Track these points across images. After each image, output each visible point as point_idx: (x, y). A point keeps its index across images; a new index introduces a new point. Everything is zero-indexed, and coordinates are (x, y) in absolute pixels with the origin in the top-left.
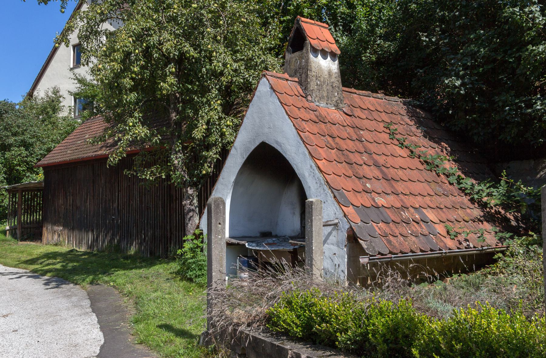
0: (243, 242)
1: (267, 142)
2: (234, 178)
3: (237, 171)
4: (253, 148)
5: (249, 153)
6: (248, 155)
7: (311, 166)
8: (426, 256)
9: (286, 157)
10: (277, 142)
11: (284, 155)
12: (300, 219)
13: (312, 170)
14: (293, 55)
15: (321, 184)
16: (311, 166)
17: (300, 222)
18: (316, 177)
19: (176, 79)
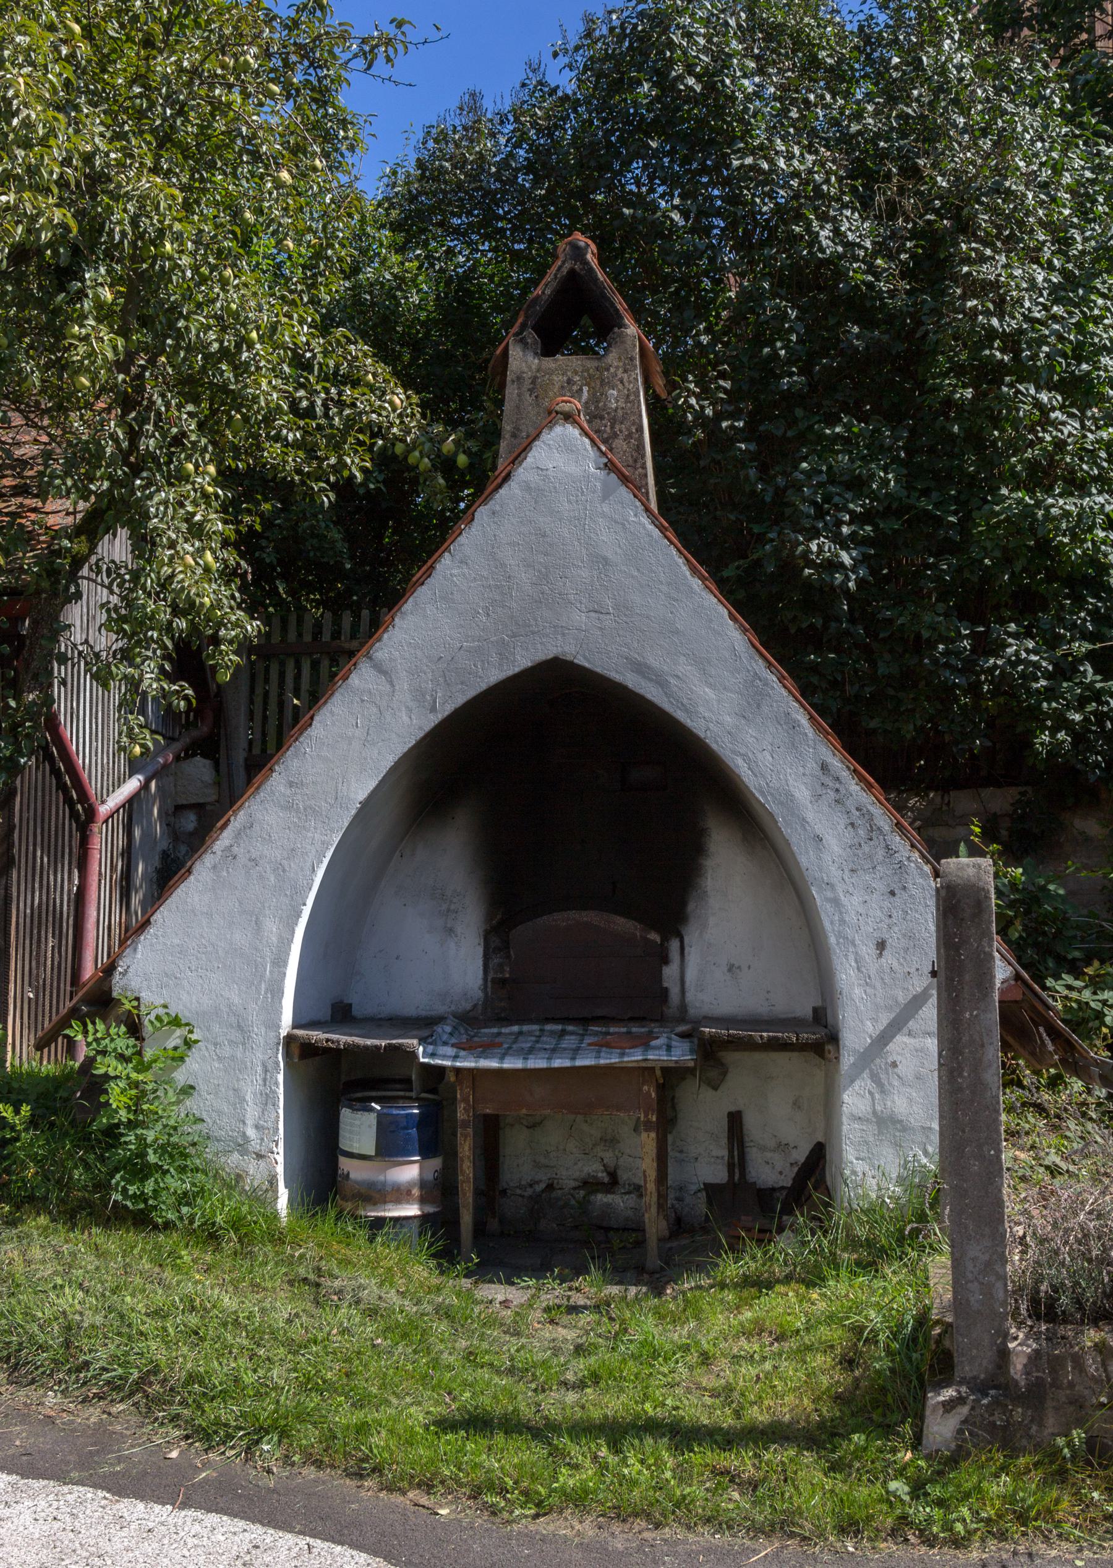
0: (409, 1041)
1: (580, 661)
2: (372, 784)
3: (389, 760)
4: (494, 675)
5: (471, 693)
6: (460, 700)
7: (824, 767)
8: (9, 1048)
9: (689, 723)
10: (641, 669)
11: (680, 716)
12: (480, 950)
13: (828, 781)
14: (549, 363)
15: (873, 829)
16: (824, 767)
17: (480, 963)
18: (850, 804)
19: (566, 82)
